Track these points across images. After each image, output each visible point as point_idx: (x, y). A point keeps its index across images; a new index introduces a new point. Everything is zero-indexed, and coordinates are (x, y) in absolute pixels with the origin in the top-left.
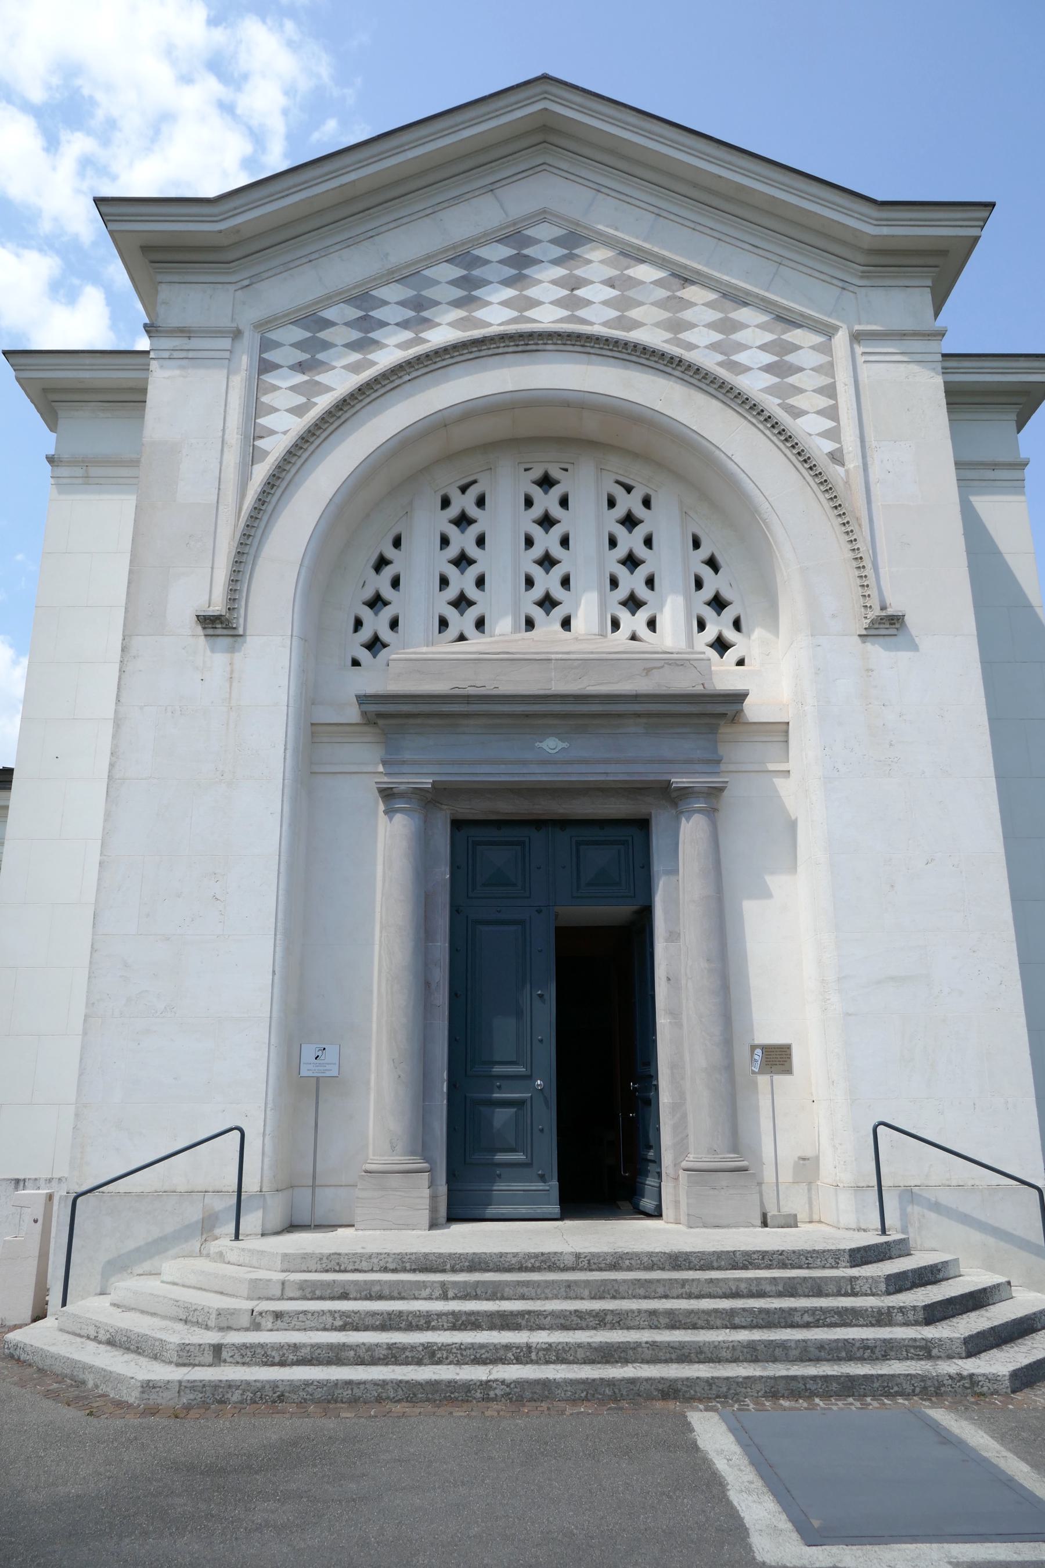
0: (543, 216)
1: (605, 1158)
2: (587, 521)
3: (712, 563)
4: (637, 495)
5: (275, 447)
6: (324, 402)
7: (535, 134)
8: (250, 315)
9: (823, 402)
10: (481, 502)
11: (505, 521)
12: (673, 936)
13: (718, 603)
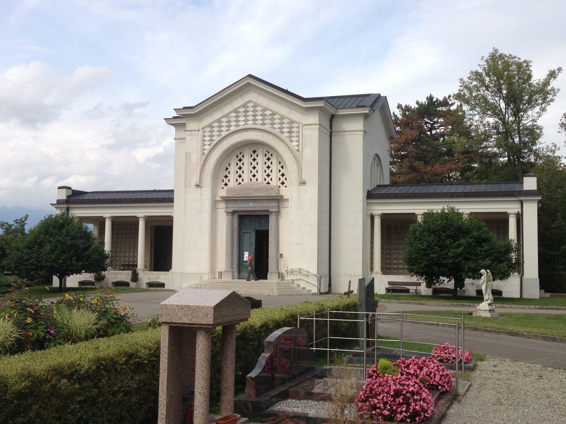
0: (250, 101)
1: (260, 268)
2: (261, 159)
3: (282, 167)
4: (270, 154)
5: (206, 152)
6: (214, 143)
8: (202, 126)
9: (297, 139)
10: (243, 156)
11: (247, 160)
13: (283, 175)
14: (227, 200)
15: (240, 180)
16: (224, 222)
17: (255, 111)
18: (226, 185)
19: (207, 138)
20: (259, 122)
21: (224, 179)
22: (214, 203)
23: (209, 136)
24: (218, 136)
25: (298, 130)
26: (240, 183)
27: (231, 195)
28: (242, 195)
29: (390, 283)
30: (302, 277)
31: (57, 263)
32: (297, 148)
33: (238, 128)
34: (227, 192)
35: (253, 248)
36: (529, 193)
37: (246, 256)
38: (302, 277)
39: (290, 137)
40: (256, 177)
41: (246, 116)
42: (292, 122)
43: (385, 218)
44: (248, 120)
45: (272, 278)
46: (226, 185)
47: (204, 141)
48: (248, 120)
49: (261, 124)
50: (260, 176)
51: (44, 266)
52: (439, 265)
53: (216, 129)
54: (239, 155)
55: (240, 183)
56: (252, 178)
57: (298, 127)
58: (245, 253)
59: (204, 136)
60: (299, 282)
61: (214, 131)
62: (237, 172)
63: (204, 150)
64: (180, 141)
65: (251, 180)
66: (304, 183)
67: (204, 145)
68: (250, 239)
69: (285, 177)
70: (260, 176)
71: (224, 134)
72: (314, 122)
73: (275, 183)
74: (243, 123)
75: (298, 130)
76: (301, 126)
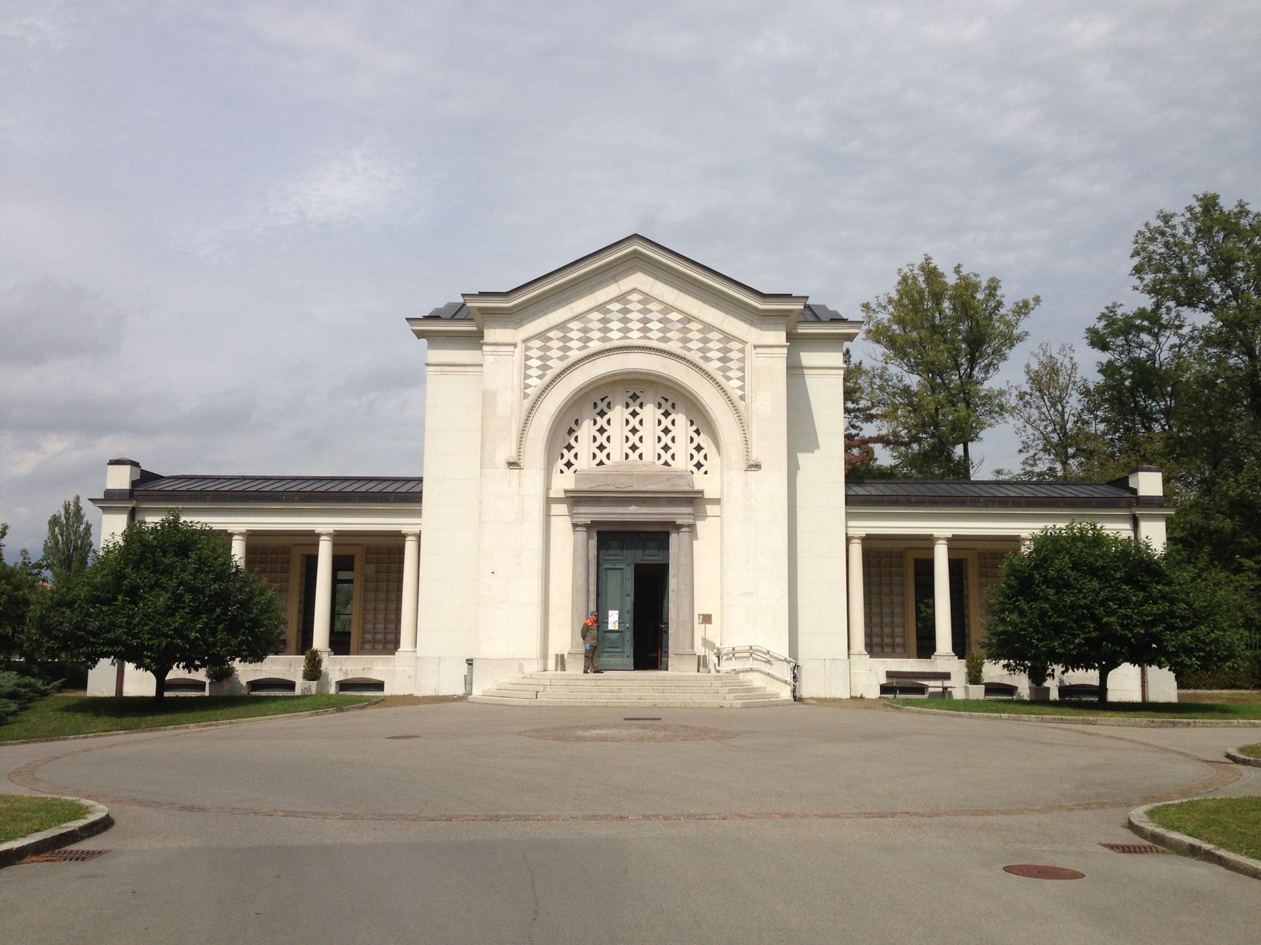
0: (634, 290)
1: (649, 647)
2: (650, 413)
3: (697, 432)
4: (670, 403)
6: (550, 374)
7: (633, 255)
9: (739, 374)
11: (618, 414)
12: (676, 576)
14: (575, 499)
15: (601, 456)
16: (568, 547)
17: (645, 311)
18: (569, 465)
19: (535, 363)
20: (655, 335)
21: (565, 451)
22: (549, 501)
23: (540, 358)
24: (561, 359)
25: (741, 355)
26: (601, 463)
27: (587, 487)
28: (612, 488)
29: (890, 675)
30: (756, 665)
31: (186, 639)
32: (740, 393)
33: (608, 345)
34: (577, 481)
35: (629, 602)
36: (1150, 502)
37: (613, 619)
38: (756, 665)
39: (725, 370)
40: (638, 452)
41: (625, 320)
42: (728, 338)
43: (867, 540)
44: (630, 330)
45: (678, 669)
46: (569, 465)
47: (527, 367)
48: (630, 330)
49: (658, 340)
50: (649, 449)
51: (149, 648)
52: (1122, 641)
53: (555, 344)
54: (599, 403)
55: (601, 463)
56: (630, 452)
57: (742, 351)
58: (611, 612)
59: (528, 358)
60: (750, 676)
61: (550, 349)
62: (595, 439)
63: (527, 386)
64: (438, 368)
65: (627, 456)
66: (757, 466)
67: (527, 377)
68: (623, 583)
69: (703, 453)
70: (649, 449)
71: (574, 355)
72: (776, 343)
73: (682, 463)
74: (618, 335)
75: (741, 355)
76: (748, 348)
